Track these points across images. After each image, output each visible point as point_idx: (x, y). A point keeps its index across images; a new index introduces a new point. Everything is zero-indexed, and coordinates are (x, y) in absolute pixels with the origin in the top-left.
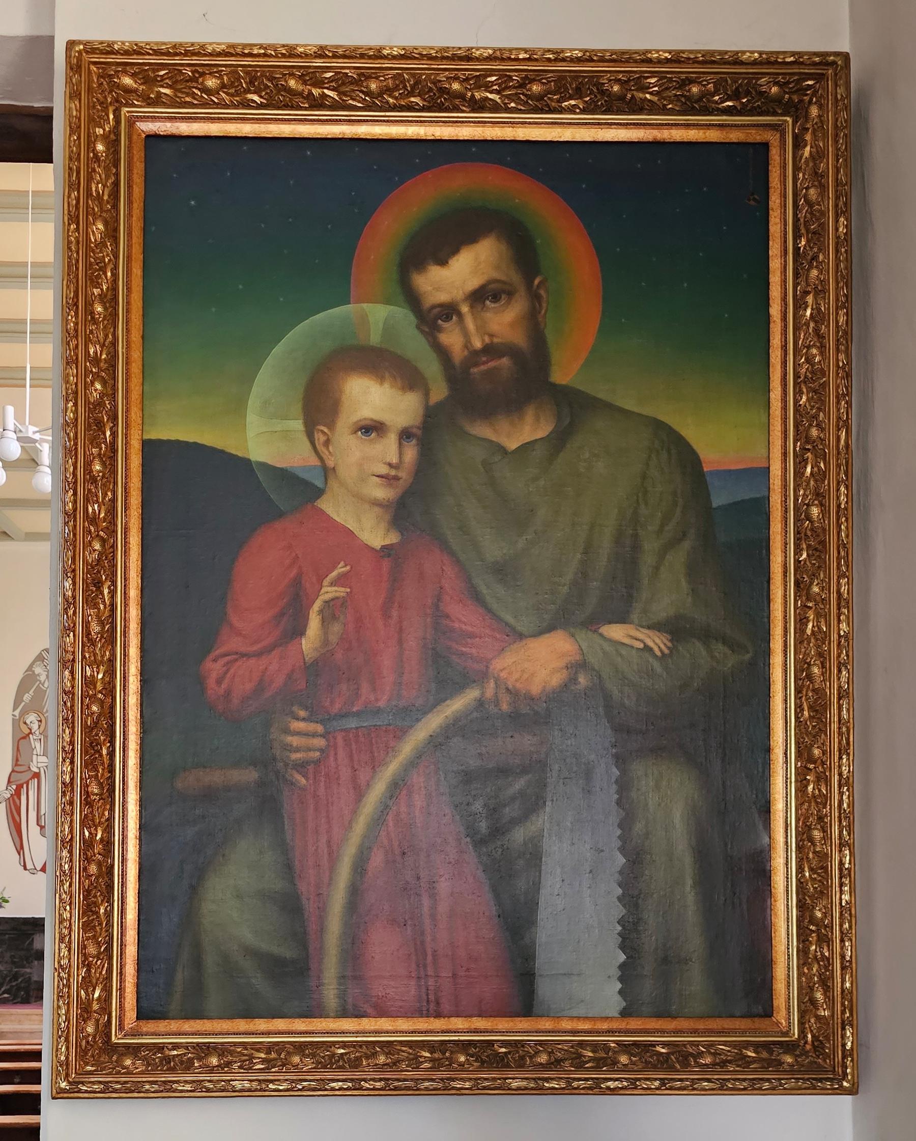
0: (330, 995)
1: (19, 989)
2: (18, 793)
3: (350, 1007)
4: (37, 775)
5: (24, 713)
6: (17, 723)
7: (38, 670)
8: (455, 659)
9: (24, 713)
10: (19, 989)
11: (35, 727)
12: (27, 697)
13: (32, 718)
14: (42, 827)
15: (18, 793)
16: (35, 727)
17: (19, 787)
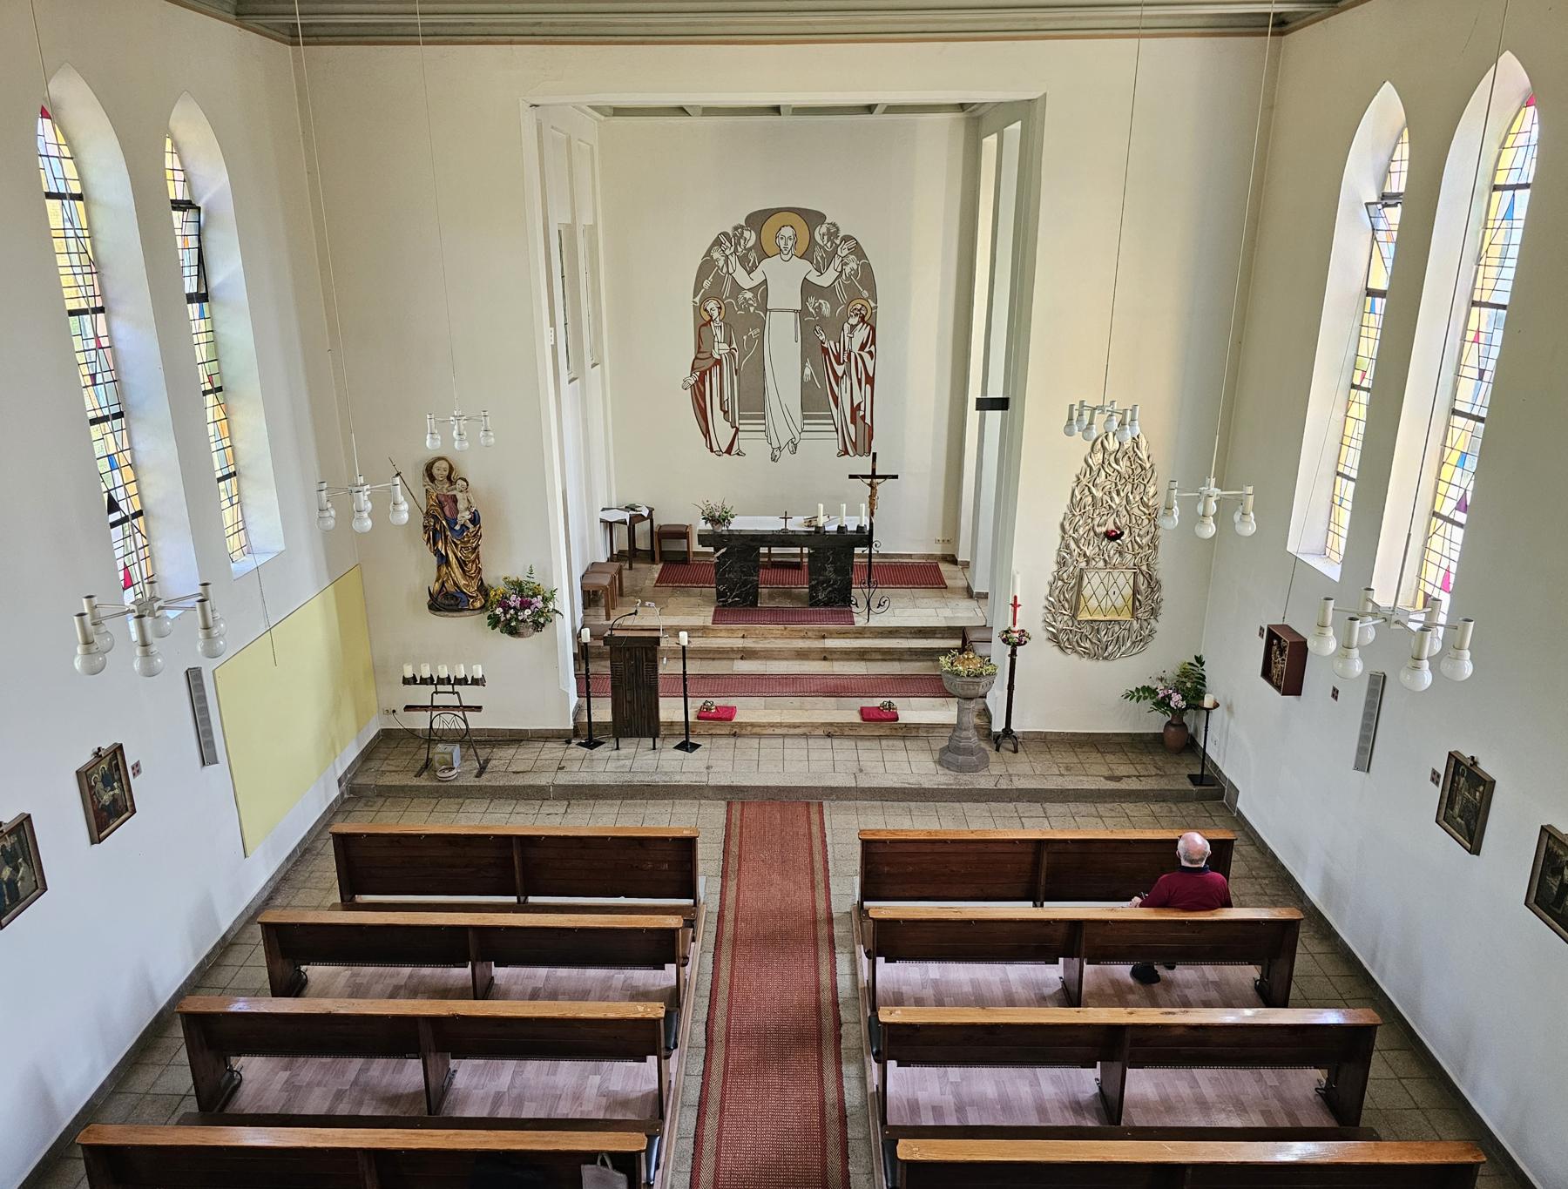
0: (884, 909)
1: (748, 594)
2: (702, 379)
3: (1154, 723)
4: (719, 362)
5: (705, 300)
6: (699, 309)
7: (716, 255)
8: (1153, 771)
9: (705, 300)
10: (748, 594)
11: (715, 314)
12: (707, 284)
13: (712, 305)
14: (725, 413)
15: (702, 379)
16: (715, 314)
17: (703, 374)
